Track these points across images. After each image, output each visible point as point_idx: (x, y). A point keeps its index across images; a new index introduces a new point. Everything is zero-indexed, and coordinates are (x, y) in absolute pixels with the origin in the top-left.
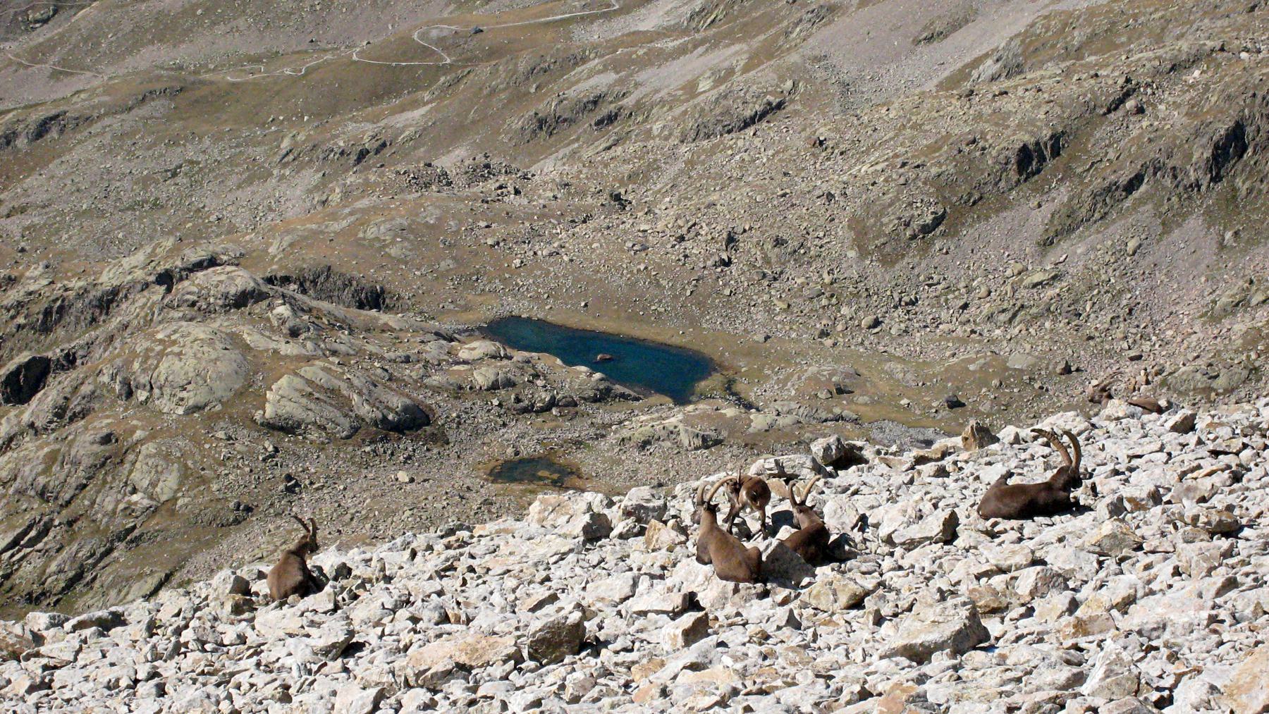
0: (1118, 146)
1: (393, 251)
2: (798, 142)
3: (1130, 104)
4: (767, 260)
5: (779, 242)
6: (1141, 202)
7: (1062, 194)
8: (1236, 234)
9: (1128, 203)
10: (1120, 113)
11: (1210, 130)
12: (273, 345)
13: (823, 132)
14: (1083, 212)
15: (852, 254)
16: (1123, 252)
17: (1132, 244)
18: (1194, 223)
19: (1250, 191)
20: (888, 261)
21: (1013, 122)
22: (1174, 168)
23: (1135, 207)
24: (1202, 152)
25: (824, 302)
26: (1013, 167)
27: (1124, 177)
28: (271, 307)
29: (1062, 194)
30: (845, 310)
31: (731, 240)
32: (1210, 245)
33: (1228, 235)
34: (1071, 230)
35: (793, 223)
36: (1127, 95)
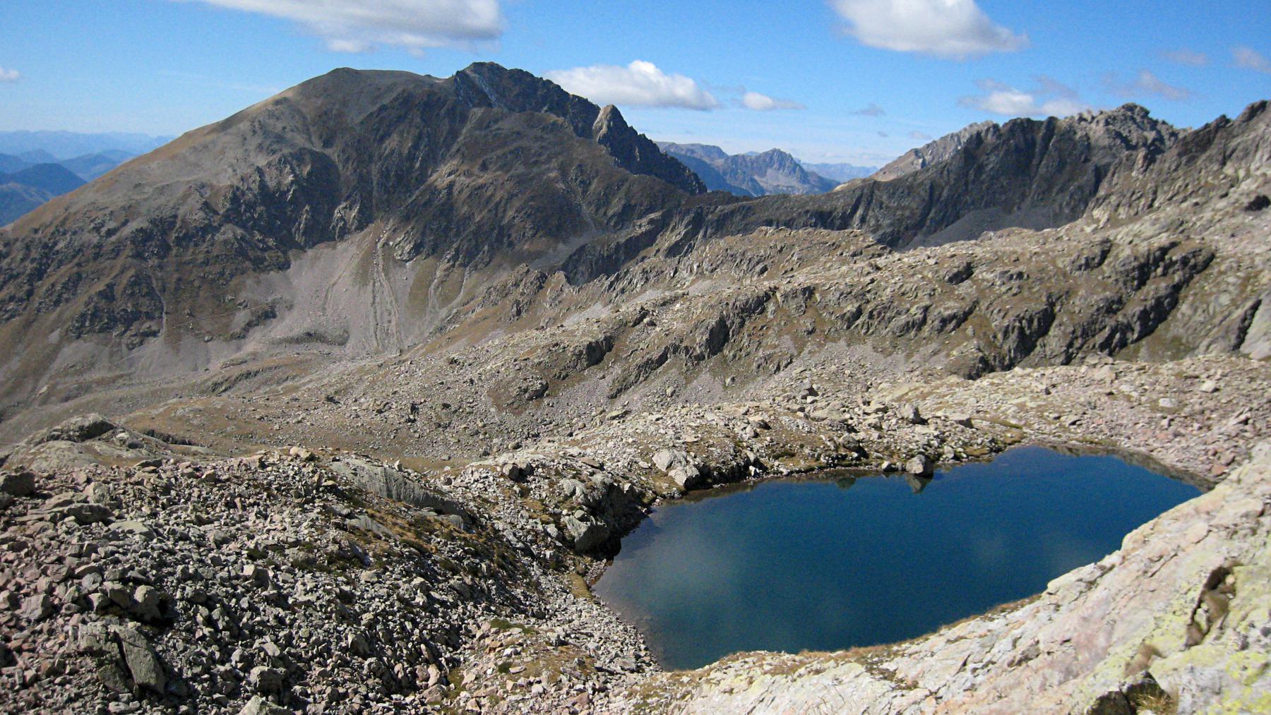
0: (649, 342)
1: (195, 422)
2: (442, 363)
3: (645, 320)
4: (438, 416)
5: (446, 406)
6: (670, 367)
7: (617, 370)
8: (733, 379)
9: (660, 369)
10: (642, 325)
11: (705, 324)
12: (119, 452)
13: (455, 356)
14: (632, 378)
15: (493, 410)
16: (665, 394)
17: (669, 391)
18: (705, 376)
19: (735, 356)
20: (517, 411)
21: (579, 333)
22: (686, 348)
23: (665, 372)
24: (701, 337)
25: (481, 437)
26: (584, 356)
27: (655, 355)
28: (114, 434)
29: (617, 370)
30: (495, 440)
31: (414, 408)
32: (718, 387)
33: (728, 380)
34: (626, 388)
35: (452, 397)
36: (643, 317)
